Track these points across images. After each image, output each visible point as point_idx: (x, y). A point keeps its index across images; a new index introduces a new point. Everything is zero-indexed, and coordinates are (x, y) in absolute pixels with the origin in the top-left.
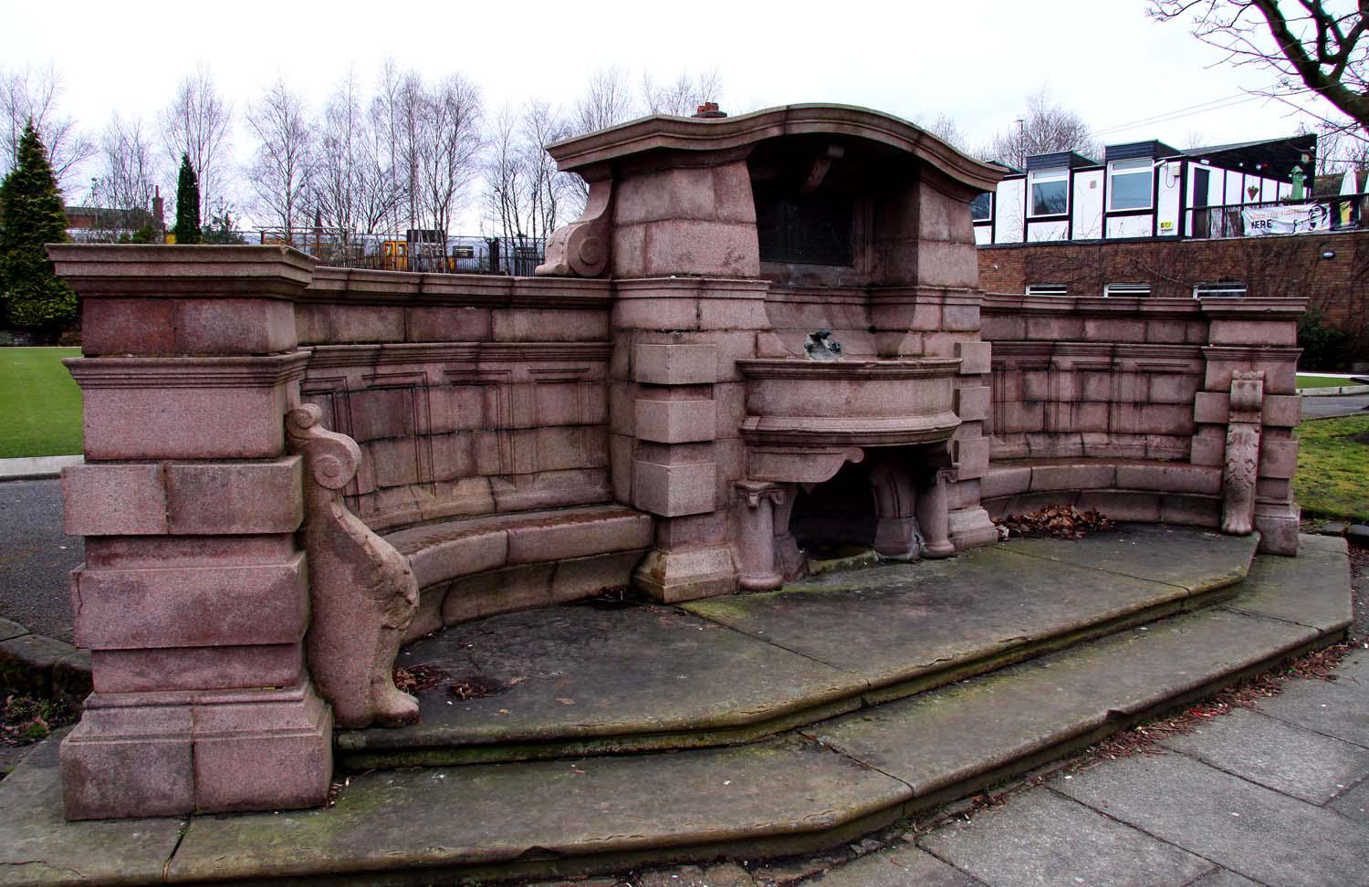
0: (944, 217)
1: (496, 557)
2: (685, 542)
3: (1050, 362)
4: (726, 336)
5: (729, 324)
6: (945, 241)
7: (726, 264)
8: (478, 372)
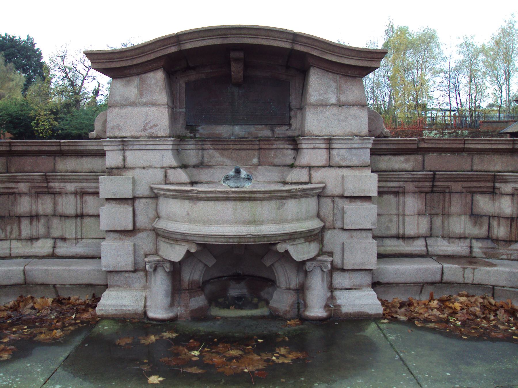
0: (333, 88)
1: (19, 279)
2: (118, 286)
3: (494, 188)
4: (144, 171)
5: (145, 164)
6: (333, 104)
7: (144, 130)
8: (47, 187)
